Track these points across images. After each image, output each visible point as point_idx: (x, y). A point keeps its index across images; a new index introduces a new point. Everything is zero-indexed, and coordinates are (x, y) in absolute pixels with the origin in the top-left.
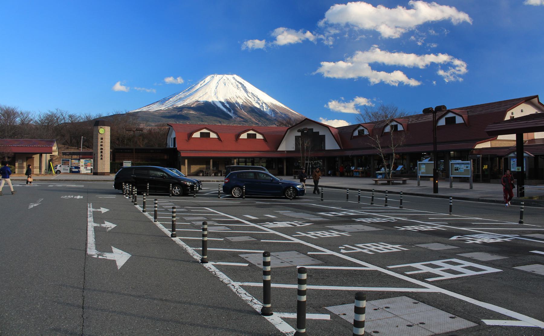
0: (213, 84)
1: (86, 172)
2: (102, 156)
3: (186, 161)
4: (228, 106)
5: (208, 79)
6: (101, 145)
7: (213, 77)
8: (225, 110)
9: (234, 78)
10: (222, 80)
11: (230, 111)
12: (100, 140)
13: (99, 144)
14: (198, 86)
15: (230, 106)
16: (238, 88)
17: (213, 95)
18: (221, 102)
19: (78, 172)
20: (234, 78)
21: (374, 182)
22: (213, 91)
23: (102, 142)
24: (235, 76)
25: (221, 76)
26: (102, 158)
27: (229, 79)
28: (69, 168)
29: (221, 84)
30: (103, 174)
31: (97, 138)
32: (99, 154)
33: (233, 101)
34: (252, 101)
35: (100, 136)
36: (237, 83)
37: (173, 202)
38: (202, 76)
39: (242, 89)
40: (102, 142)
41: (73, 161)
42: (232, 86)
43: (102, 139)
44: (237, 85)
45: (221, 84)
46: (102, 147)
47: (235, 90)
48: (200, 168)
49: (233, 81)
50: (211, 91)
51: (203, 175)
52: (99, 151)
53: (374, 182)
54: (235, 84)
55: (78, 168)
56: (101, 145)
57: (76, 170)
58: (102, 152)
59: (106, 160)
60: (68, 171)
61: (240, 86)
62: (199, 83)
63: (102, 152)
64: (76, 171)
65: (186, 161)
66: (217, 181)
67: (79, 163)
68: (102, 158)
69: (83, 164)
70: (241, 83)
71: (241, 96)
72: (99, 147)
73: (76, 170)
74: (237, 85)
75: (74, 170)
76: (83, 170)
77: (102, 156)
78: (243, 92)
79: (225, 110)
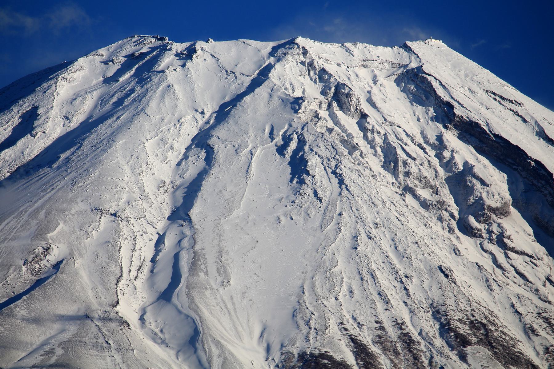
0: (145, 162)
5: (74, 89)
7: (144, 68)
9: (416, 84)
10: (257, 105)
16: (471, 214)
20: (416, 84)
21: (381, 122)
22: (137, 246)
24: (436, 57)
25: (242, 54)
27: (358, 85)
29: (250, 170)
36: (463, 153)
37: (14, 218)
42: (386, 187)
44: (460, 181)
45: (250, 170)
47: (435, 239)
49: (403, 116)
50: (110, 246)
53: (381, 122)
54: (424, 165)
66: (118, 118)
74: (460, 181)
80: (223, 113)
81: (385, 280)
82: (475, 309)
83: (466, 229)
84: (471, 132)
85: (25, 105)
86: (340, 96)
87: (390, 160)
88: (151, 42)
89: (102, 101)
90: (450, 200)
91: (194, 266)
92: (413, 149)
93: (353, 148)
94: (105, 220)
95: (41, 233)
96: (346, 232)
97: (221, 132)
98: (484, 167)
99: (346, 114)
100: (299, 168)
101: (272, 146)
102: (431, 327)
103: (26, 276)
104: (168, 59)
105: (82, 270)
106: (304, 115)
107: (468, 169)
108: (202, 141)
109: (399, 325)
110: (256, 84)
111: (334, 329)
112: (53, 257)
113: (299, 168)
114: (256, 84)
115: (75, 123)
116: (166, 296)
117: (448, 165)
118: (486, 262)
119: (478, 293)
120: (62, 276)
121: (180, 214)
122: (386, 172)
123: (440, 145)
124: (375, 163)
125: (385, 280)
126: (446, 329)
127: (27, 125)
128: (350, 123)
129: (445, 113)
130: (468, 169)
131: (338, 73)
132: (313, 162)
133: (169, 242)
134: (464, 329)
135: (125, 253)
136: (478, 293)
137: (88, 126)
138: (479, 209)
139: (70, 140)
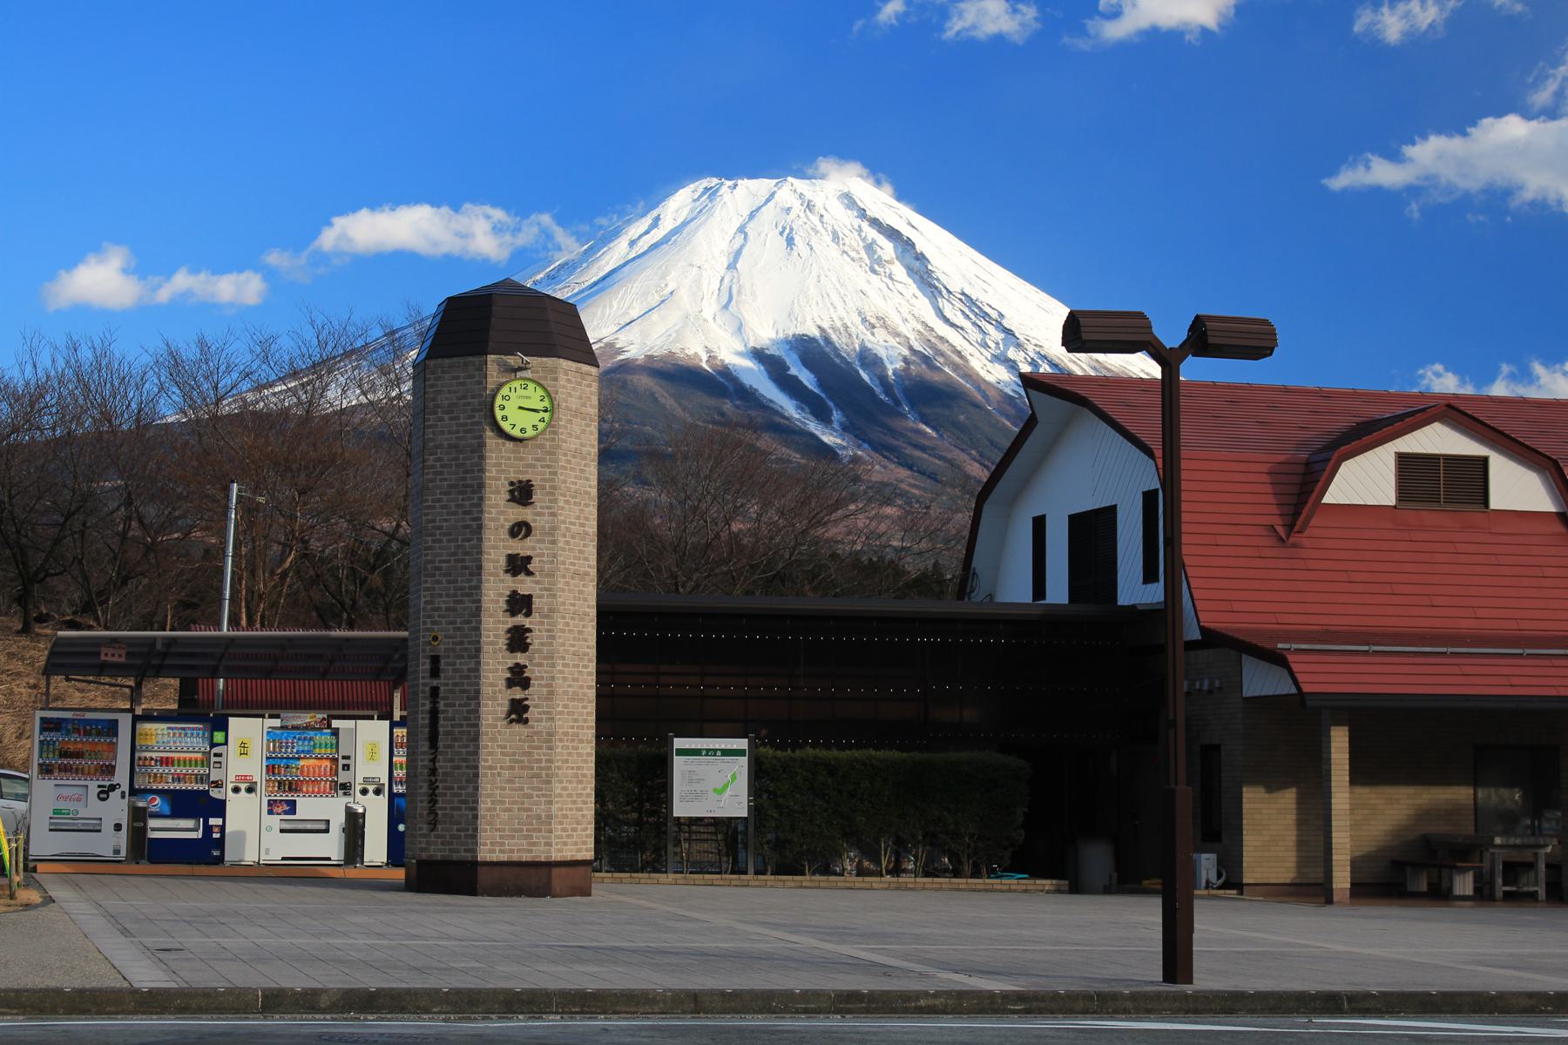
0: (714, 240)
1: (277, 846)
2: (518, 678)
3: (1339, 742)
4: (807, 378)
5: (678, 205)
6: (518, 565)
7: (711, 193)
8: (788, 406)
9: (849, 200)
11: (823, 416)
12: (498, 512)
13: (496, 548)
14: (617, 253)
15: (821, 383)
16: (875, 264)
17: (710, 308)
18: (759, 355)
19: (207, 853)
20: (849, 200)
22: (711, 283)
23: (520, 530)
25: (762, 186)
26: (518, 711)
27: (819, 202)
28: (117, 809)
30: (531, 879)
31: (474, 489)
32: (495, 664)
33: (846, 345)
34: (966, 349)
35: (500, 467)
36: (872, 233)
38: (648, 189)
39: (899, 271)
40: (520, 530)
41: (157, 733)
43: (522, 493)
44: (870, 248)
46: (525, 585)
47: (858, 276)
48: (1423, 815)
49: (844, 218)
50: (698, 283)
51: (1483, 894)
52: (495, 625)
54: (853, 240)
55: (201, 804)
56: (518, 565)
57: (186, 829)
58: (518, 640)
59: (563, 725)
60: (112, 843)
61: (887, 248)
62: (615, 234)
63: (518, 640)
64: (181, 843)
65: (1339, 742)
67: (213, 754)
68: (518, 711)
69: (254, 767)
70: (892, 234)
71: (895, 319)
72: (496, 587)
73: (186, 829)
74: (870, 248)
75: (165, 828)
76: (252, 830)
77: (518, 678)
78: (911, 288)
79: (788, 406)
80: (752, 216)
81: (835, 297)
82: (1515, 856)
83: (874, 271)
84: (875, 223)
85: (655, 213)
86: (810, 206)
87: (836, 237)
88: (715, 181)
89: (692, 211)
90: (865, 256)
91: (739, 292)
92: (846, 232)
93: (817, 232)
94: (695, 269)
95: (663, 277)
96: (814, 274)
97: (751, 225)
98: (882, 240)
99: (809, 178)
100: (790, 242)
101: (777, 232)
102: (858, 320)
103: (657, 299)
104: (724, 189)
105: (684, 297)
106: (792, 215)
107: (874, 242)
108: (741, 229)
109: (841, 319)
110: (768, 201)
111: (809, 323)
112: (670, 289)
113: (790, 242)
114: (768, 201)
115: (679, 222)
116: (726, 307)
117: (864, 240)
118: (884, 287)
119: (880, 302)
120: (675, 298)
121: (732, 266)
122: (486, 690)
123: (860, 230)
124: (828, 239)
125: (835, 297)
126: (864, 320)
127: (656, 223)
128: (815, 219)
129: (862, 214)
130: (874, 242)
131: (809, 195)
132: (797, 239)
133: (726, 280)
134: (873, 321)
135: (705, 287)
136: (880, 302)
137: (685, 224)
138: (879, 261)
139: (676, 231)
